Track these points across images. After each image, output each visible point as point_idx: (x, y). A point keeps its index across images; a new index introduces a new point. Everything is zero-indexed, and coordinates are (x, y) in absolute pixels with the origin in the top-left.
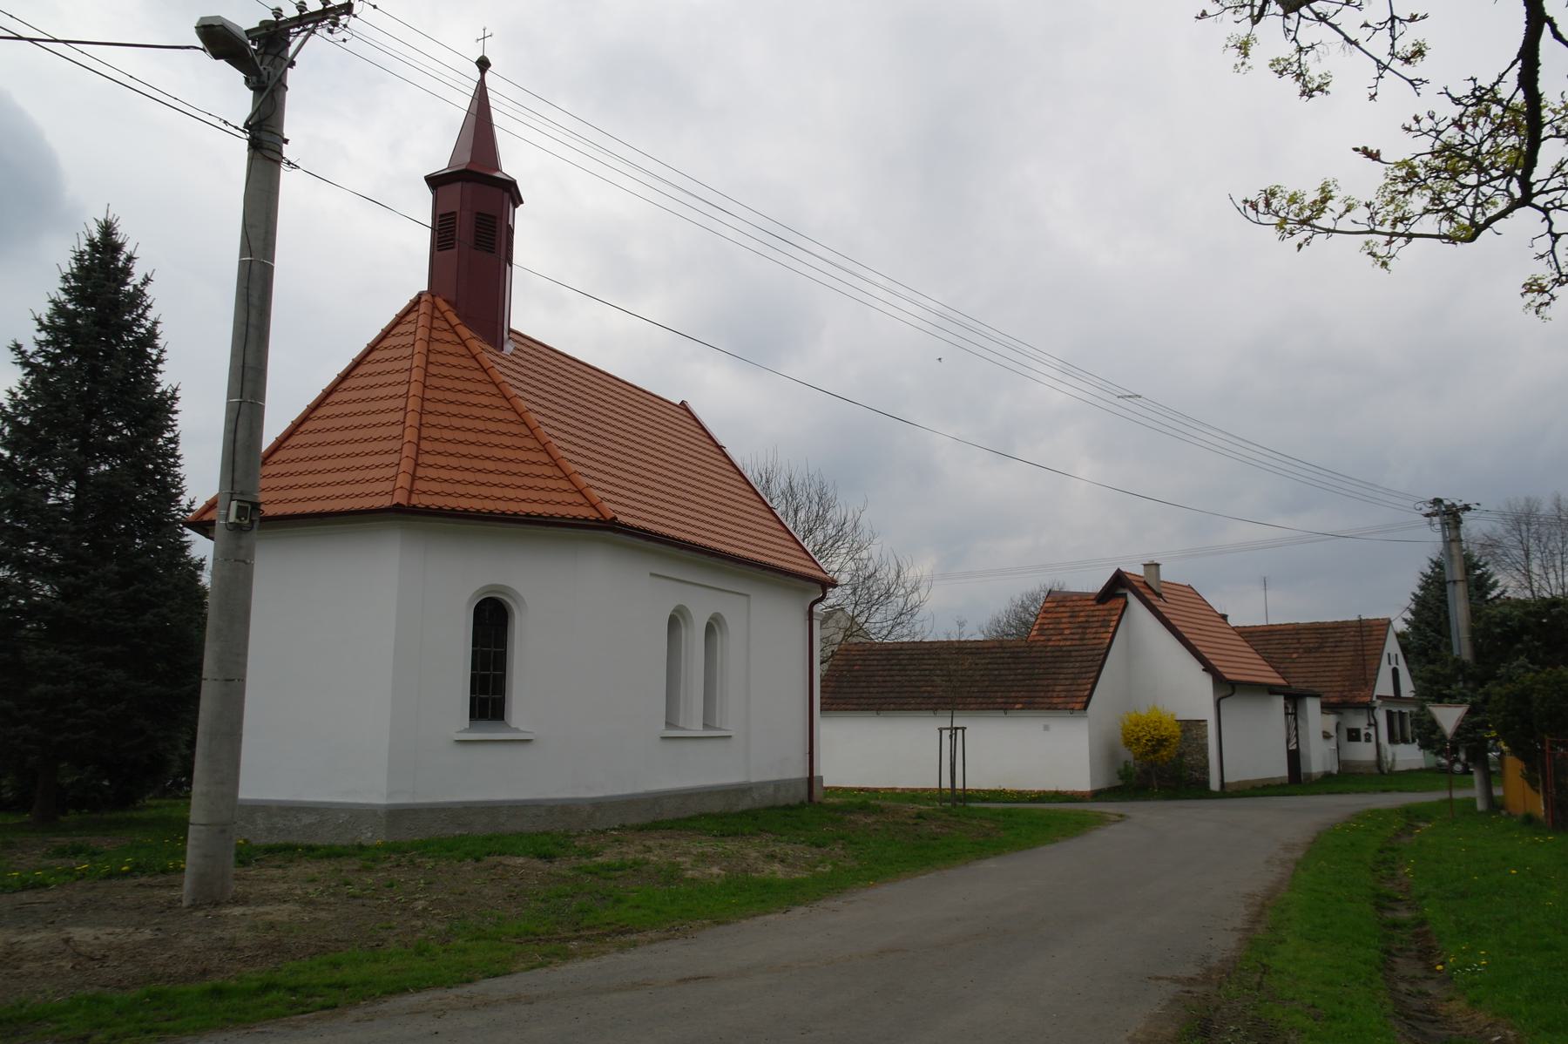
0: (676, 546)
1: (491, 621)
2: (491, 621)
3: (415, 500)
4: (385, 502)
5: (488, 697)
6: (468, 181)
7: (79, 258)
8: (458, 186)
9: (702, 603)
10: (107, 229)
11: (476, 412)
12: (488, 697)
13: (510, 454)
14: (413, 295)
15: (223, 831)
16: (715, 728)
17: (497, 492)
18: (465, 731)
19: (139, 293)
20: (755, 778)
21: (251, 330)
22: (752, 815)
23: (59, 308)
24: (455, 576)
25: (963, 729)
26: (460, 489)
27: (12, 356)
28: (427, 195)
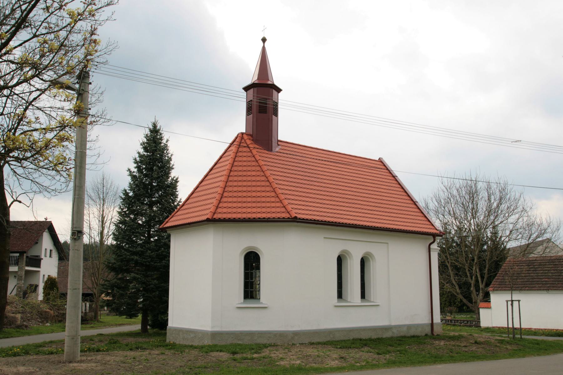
0: (337, 226)
1: (252, 261)
2: (252, 261)
3: (215, 216)
4: (204, 218)
5: (251, 290)
6: (255, 87)
7: (147, 136)
8: (252, 89)
9: (356, 248)
10: (155, 125)
11: (249, 178)
12: (251, 290)
13: (259, 194)
14: (236, 135)
15: (73, 339)
16: (371, 302)
17: (249, 210)
18: (241, 303)
19: (166, 146)
20: (394, 323)
21: (77, 174)
22: (354, 341)
23: (141, 156)
24: (237, 243)
25: (519, 301)
26: (234, 210)
27: (128, 173)
28: (244, 93)
